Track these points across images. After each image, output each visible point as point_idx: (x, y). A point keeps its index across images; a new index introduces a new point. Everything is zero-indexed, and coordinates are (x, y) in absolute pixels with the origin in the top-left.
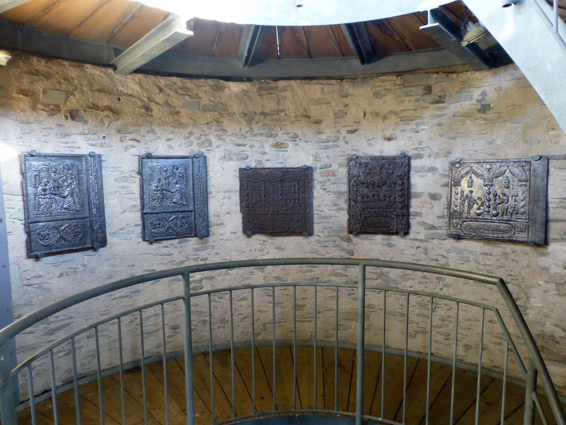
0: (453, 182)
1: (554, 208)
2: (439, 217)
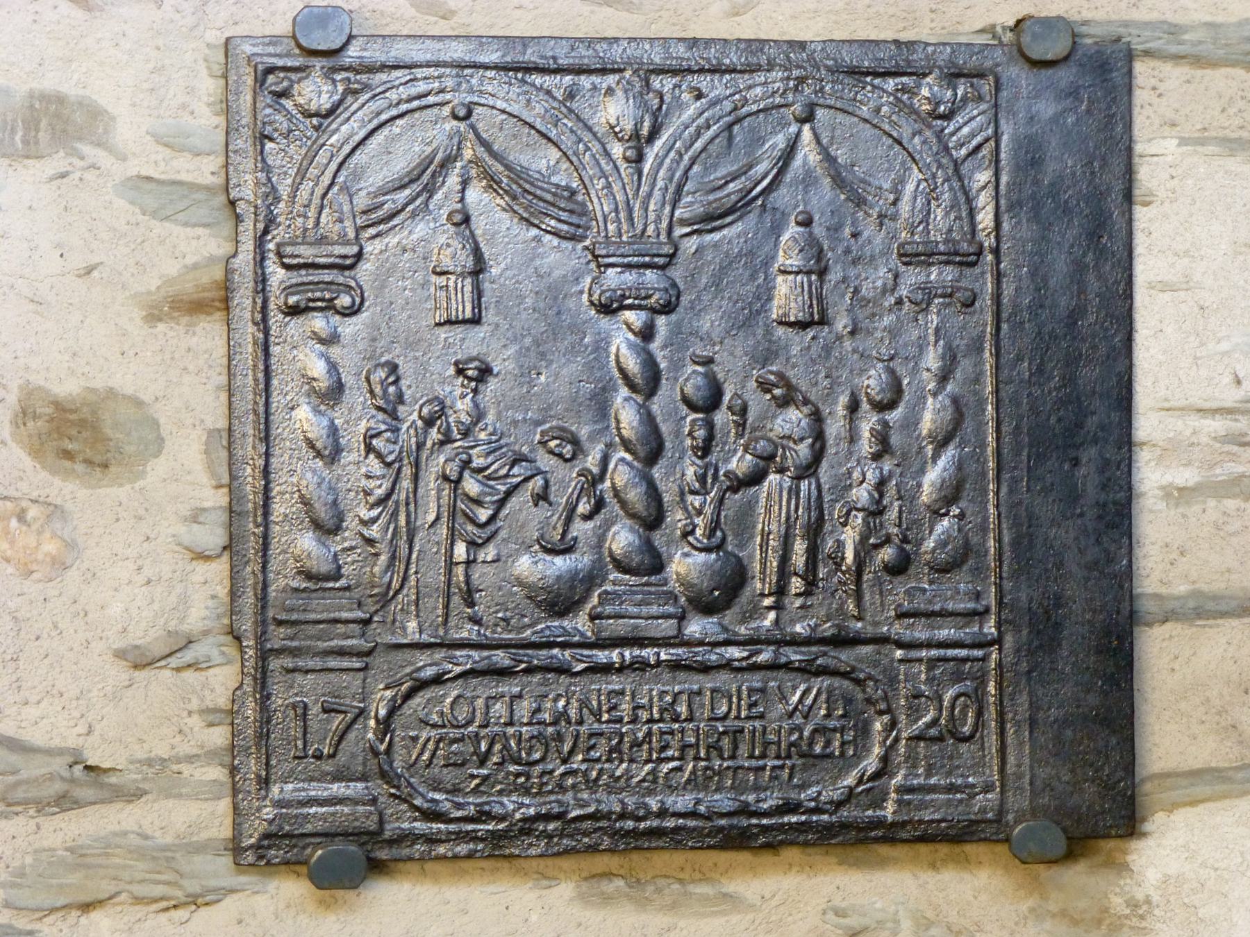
0: (277, 275)
1: (1179, 495)
2: (140, 660)
